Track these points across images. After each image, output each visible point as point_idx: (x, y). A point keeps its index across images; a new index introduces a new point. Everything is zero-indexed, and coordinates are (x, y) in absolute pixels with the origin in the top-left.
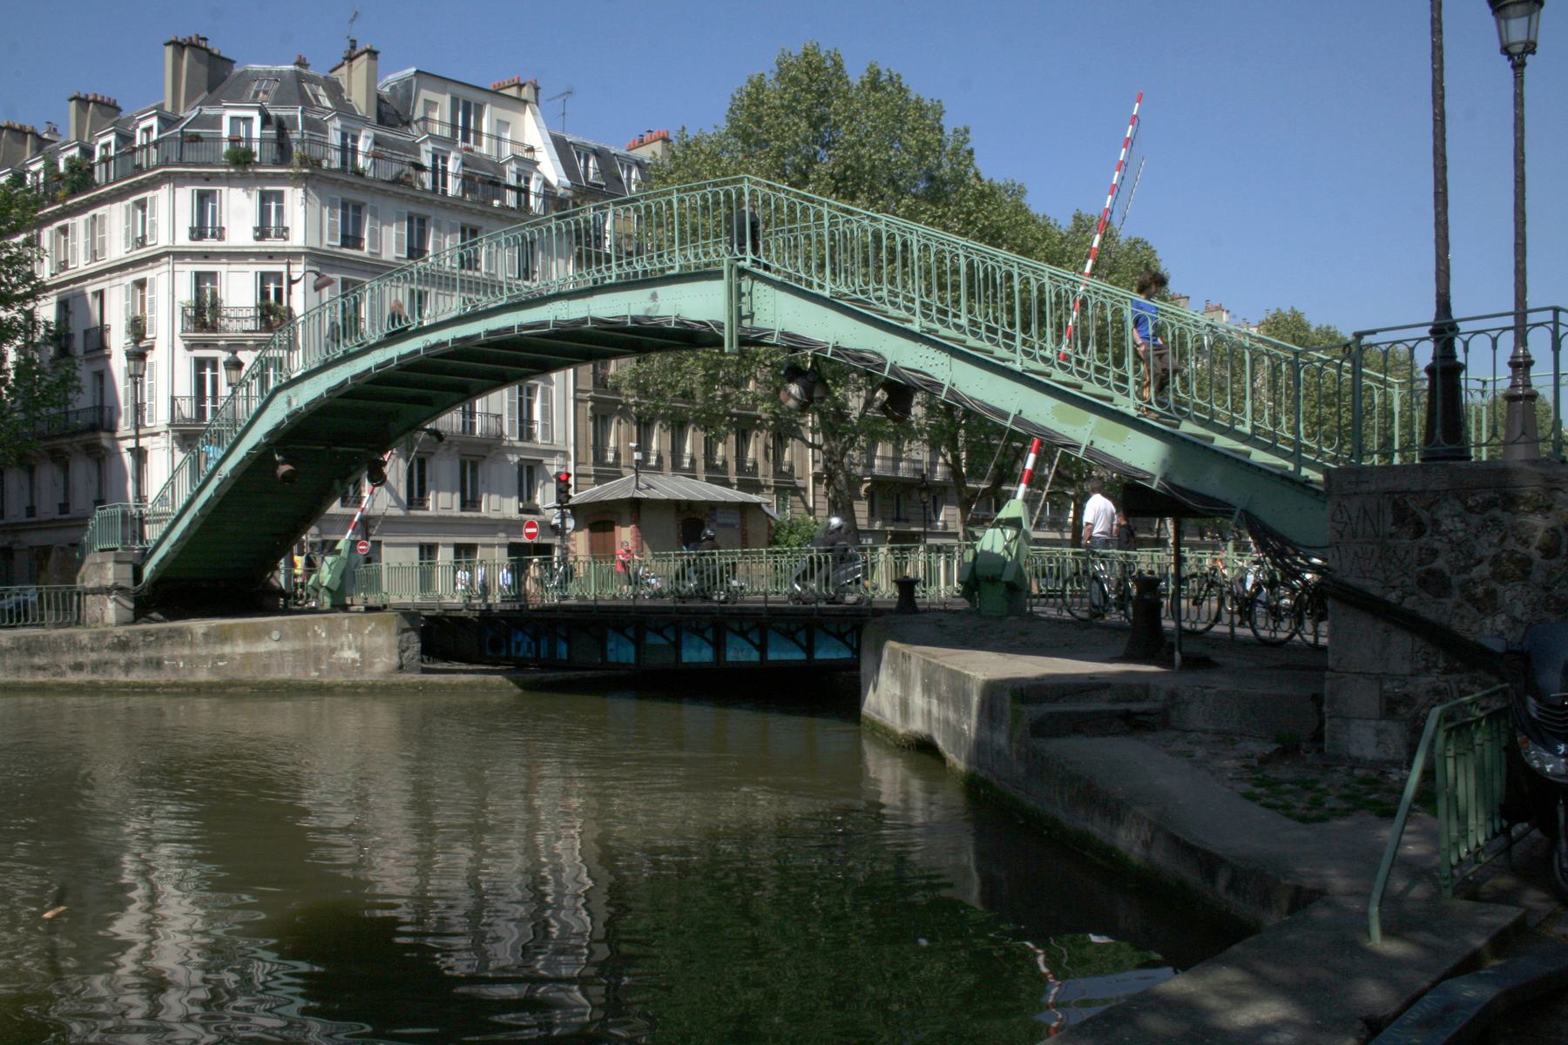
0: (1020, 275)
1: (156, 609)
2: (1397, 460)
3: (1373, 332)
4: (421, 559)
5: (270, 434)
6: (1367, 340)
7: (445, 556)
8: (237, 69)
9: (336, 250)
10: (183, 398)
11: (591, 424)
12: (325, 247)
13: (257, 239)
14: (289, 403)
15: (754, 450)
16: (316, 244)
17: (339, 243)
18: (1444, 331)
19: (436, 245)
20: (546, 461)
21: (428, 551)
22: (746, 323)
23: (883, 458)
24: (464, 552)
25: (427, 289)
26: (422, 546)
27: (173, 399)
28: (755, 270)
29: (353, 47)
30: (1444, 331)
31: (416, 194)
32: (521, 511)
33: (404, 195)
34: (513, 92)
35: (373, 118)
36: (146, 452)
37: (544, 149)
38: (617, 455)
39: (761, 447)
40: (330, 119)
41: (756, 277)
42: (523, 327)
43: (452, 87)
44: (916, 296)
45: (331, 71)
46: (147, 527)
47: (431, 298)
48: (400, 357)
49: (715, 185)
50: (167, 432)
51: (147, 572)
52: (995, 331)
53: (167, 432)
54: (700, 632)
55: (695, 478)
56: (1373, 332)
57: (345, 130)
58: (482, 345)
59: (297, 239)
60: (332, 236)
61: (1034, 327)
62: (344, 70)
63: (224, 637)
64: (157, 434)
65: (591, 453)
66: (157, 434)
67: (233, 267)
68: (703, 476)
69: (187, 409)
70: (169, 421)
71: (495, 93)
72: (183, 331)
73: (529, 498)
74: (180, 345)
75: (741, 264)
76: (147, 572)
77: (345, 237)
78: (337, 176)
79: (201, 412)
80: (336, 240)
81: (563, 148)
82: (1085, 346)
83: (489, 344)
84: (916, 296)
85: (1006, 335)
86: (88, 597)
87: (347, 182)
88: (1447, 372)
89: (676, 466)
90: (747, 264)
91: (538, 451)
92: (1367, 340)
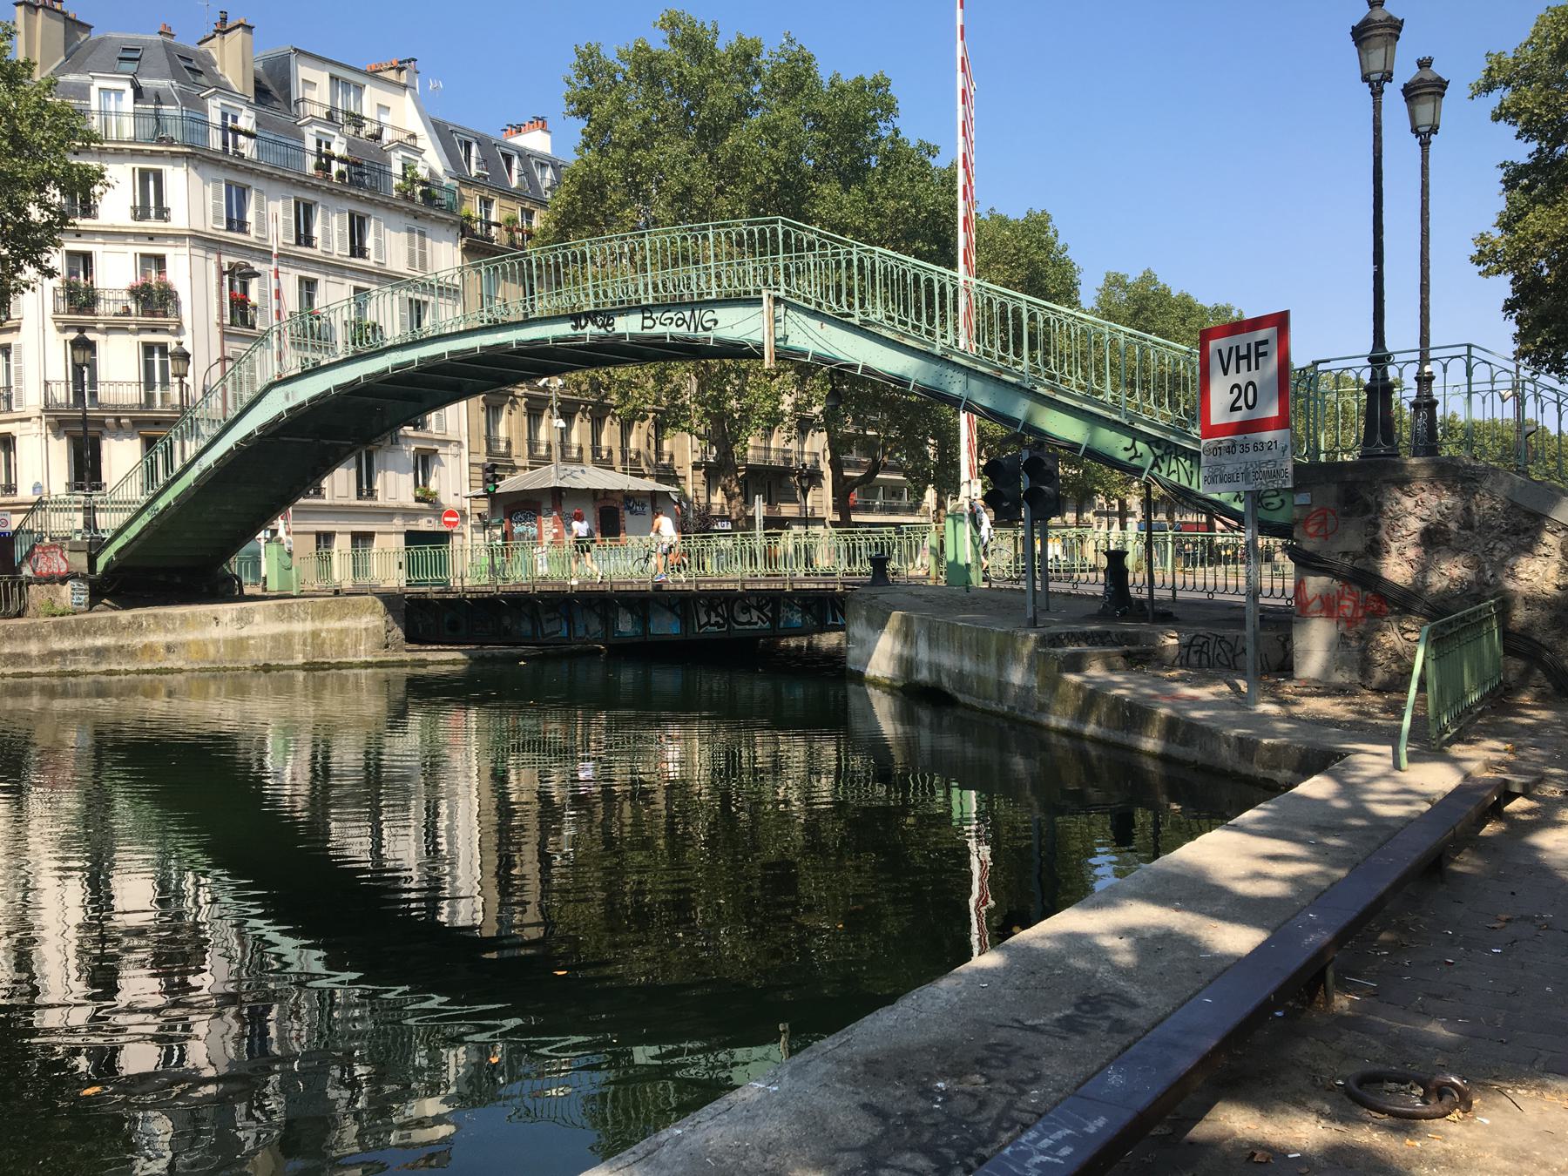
0: (1029, 311)
1: (108, 596)
2: (1323, 458)
3: (1328, 361)
4: (318, 547)
5: (263, 428)
6: (1321, 367)
7: (342, 544)
8: (95, 35)
9: (221, 233)
10: (58, 383)
11: (526, 419)
12: (210, 230)
13: (135, 218)
14: (287, 397)
15: (637, 440)
16: (201, 228)
17: (224, 227)
18: (1379, 359)
19: (260, 217)
20: (441, 450)
21: (325, 538)
22: (781, 344)
23: (755, 448)
24: (362, 539)
25: (425, 298)
26: (318, 534)
27: (47, 383)
28: (789, 299)
29: (224, 20)
30: (1379, 359)
31: (415, 208)
32: (418, 500)
33: (220, 161)
34: (392, 75)
35: (251, 93)
36: (14, 438)
37: (426, 136)
38: (509, 444)
39: (644, 438)
40: (210, 96)
41: (789, 306)
42: (556, 340)
43: (328, 66)
44: (896, 316)
45: (199, 44)
46: (97, 515)
47: (321, 286)
48: (421, 360)
49: (750, 224)
50: (40, 417)
51: (101, 562)
52: (905, 324)
53: (40, 417)
54: (671, 609)
55: (613, 469)
56: (1328, 361)
57: (226, 110)
58: (513, 352)
59: (179, 220)
60: (217, 219)
61: (937, 321)
62: (216, 41)
63: (137, 627)
64: (28, 419)
65: (484, 442)
66: (28, 419)
67: (108, 247)
68: (619, 468)
69: (61, 394)
70: (42, 407)
71: (373, 75)
72: (56, 312)
73: (425, 485)
74: (51, 327)
75: (777, 293)
76: (101, 562)
77: (230, 221)
78: (220, 157)
79: (79, 396)
80: (345, 250)
81: (443, 132)
82: (906, 310)
83: (519, 352)
84: (896, 316)
85: (914, 327)
86: (31, 587)
87: (229, 163)
88: (1380, 390)
89: (565, 458)
90: (782, 294)
91: (433, 441)
92: (1321, 367)
